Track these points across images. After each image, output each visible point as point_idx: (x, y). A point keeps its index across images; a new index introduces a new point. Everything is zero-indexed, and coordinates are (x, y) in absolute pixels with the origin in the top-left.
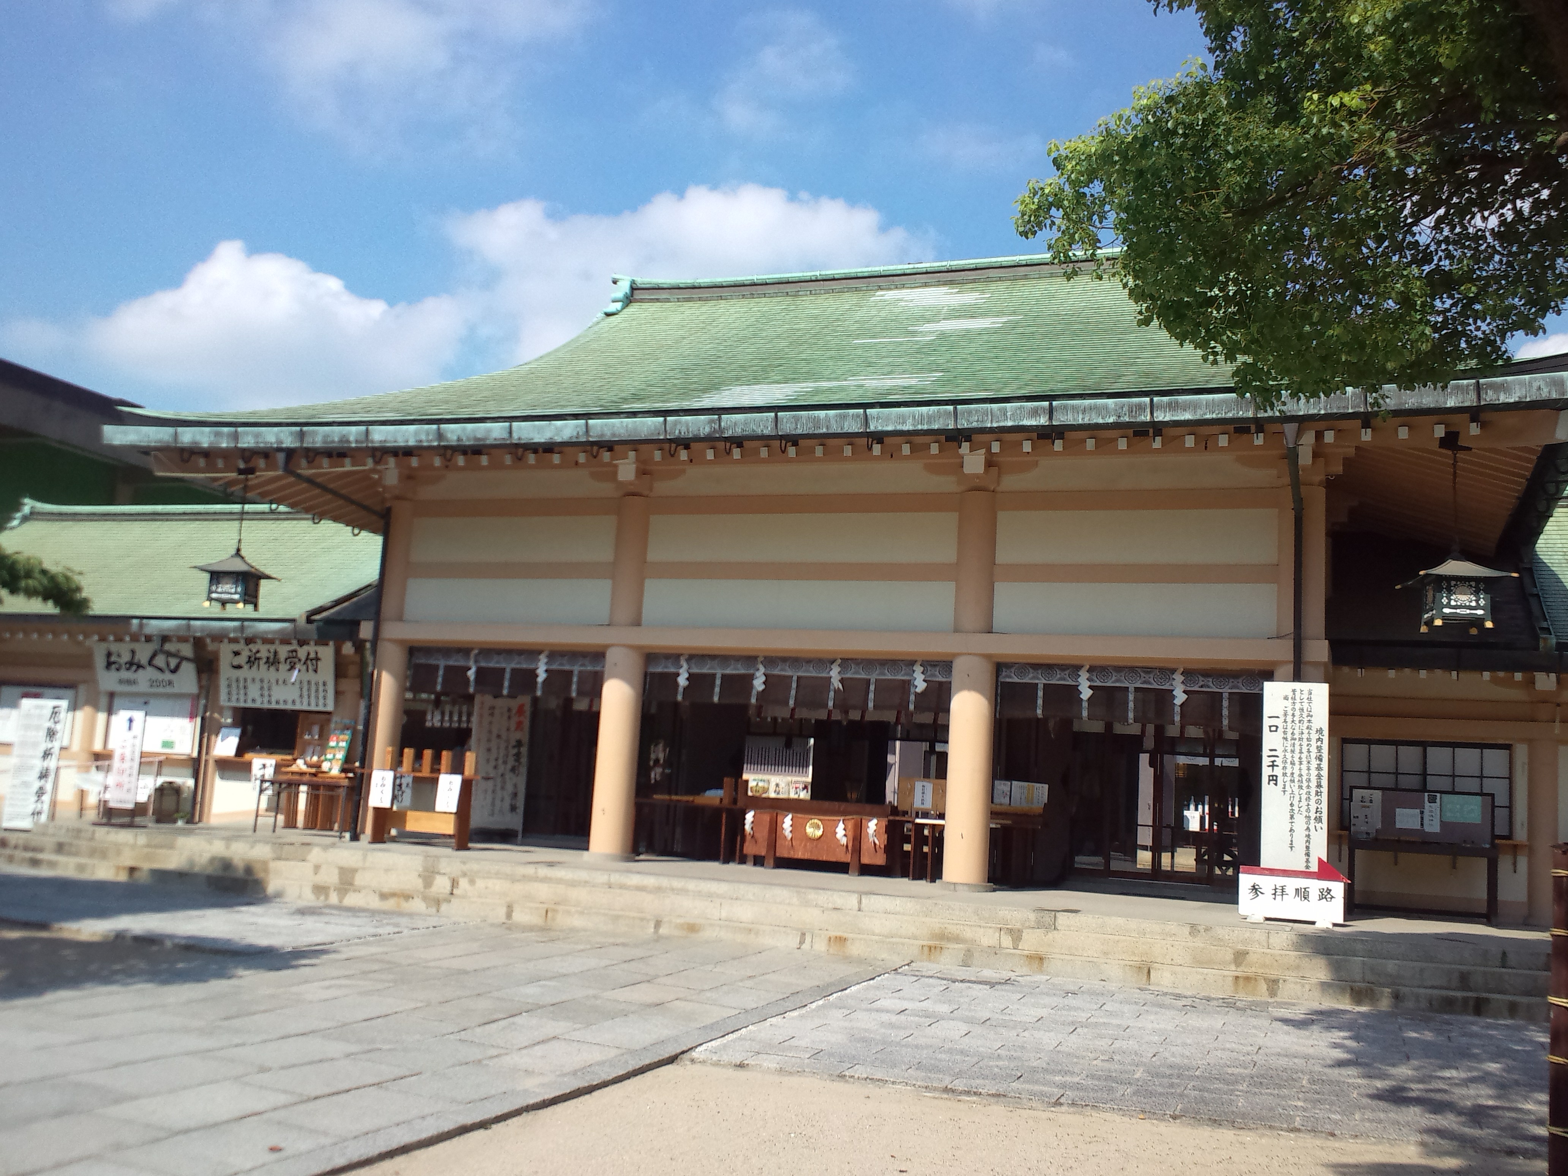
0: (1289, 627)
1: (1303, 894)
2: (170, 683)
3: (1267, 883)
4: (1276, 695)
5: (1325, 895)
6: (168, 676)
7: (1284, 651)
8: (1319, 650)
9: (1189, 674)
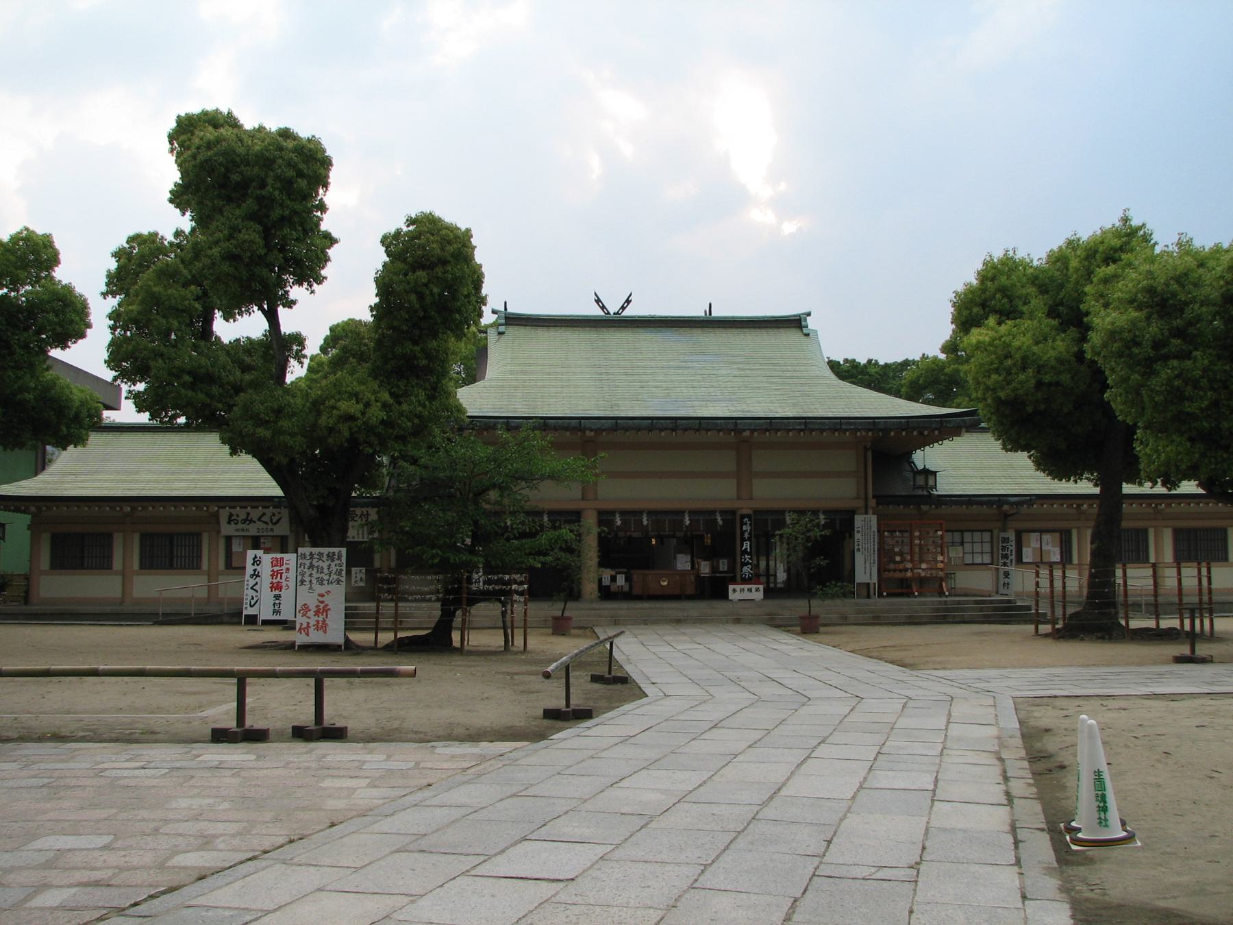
0: (863, 496)
1: (750, 590)
2: (272, 530)
3: (738, 587)
4: (859, 520)
5: (757, 590)
6: (270, 526)
7: (860, 503)
8: (872, 502)
9: (825, 512)
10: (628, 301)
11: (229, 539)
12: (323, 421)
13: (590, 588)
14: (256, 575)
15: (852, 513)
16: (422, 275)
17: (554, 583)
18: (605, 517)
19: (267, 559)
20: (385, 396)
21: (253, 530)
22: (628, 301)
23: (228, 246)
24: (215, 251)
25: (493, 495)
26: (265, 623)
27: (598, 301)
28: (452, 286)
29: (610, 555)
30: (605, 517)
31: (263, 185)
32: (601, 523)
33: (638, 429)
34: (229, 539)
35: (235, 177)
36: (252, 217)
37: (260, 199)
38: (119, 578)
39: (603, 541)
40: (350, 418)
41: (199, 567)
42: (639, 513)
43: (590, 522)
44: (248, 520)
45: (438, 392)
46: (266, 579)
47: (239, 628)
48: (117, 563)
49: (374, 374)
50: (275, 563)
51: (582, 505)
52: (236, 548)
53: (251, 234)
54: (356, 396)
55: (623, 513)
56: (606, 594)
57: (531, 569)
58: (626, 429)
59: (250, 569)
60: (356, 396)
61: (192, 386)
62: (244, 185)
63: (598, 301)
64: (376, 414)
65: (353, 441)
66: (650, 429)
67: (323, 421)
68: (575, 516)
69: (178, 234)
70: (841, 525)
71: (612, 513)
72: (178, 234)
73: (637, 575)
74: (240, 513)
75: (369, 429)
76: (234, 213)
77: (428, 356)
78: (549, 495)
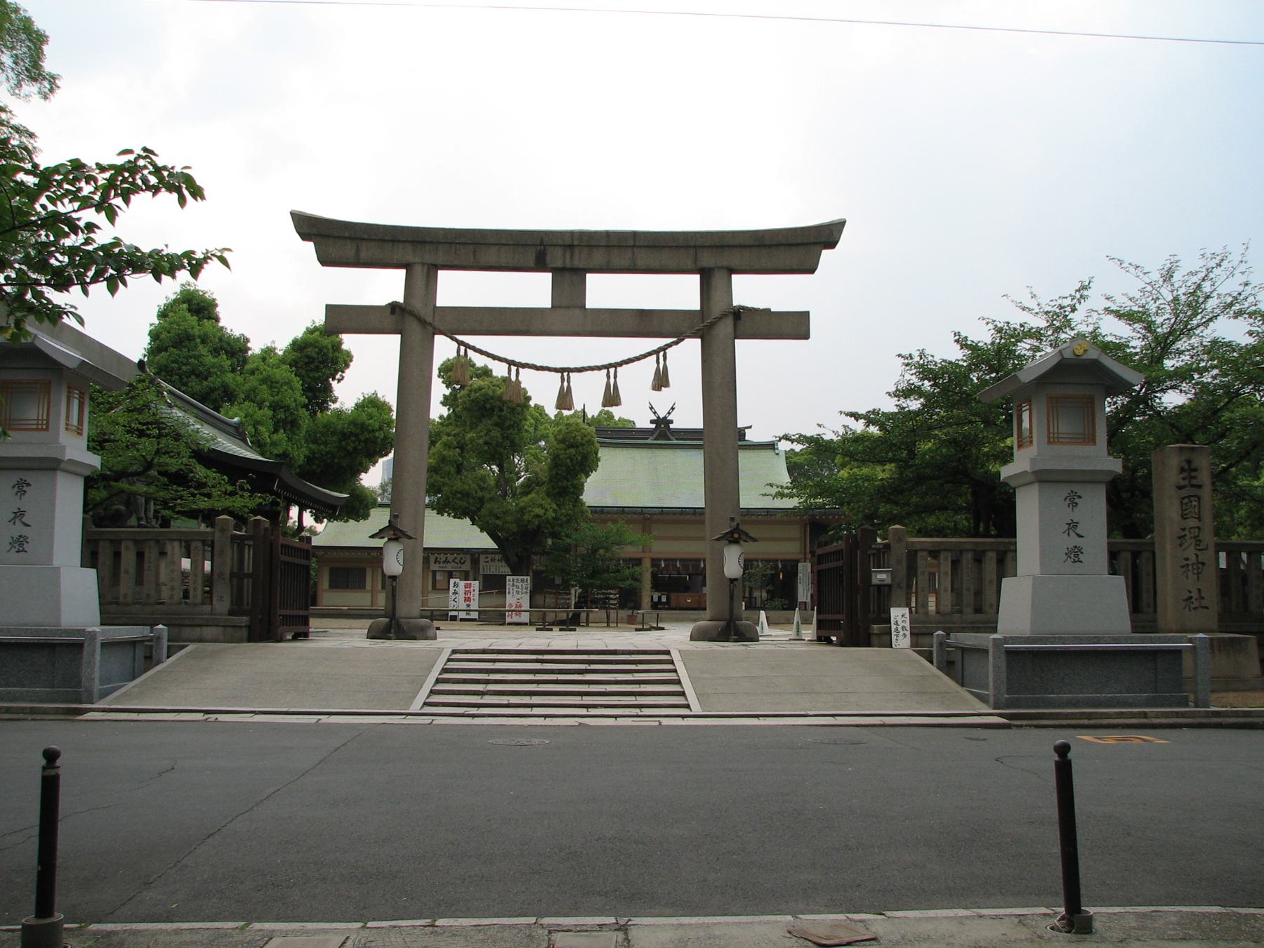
8: (809, 556)
10: (673, 409)
11: (434, 573)
12: (526, 517)
13: (646, 601)
14: (455, 593)
15: (797, 561)
16: (572, 451)
17: (629, 600)
18: (655, 562)
19: (462, 583)
20: (554, 506)
21: (449, 567)
22: (673, 409)
23: (486, 438)
24: (481, 441)
25: (601, 551)
26: (462, 620)
27: (651, 408)
28: (585, 457)
29: (657, 584)
30: (655, 562)
31: (502, 410)
32: (653, 566)
33: (674, 514)
34: (434, 573)
35: (488, 406)
36: (496, 424)
37: (499, 417)
38: (369, 595)
39: (654, 575)
40: (538, 516)
41: (364, 587)
42: (675, 560)
43: (647, 564)
44: (446, 561)
45: (577, 502)
46: (462, 596)
47: (783, 557)
48: (368, 586)
49: (548, 494)
50: (467, 586)
51: (642, 555)
52: (439, 577)
53: (496, 433)
54: (541, 506)
55: (665, 560)
56: (655, 606)
57: (620, 588)
58: (668, 514)
59: (452, 589)
60: (541, 506)
61: (460, 499)
62: (492, 409)
63: (651, 408)
64: (551, 514)
65: (539, 527)
66: (681, 513)
67: (526, 517)
68: (638, 562)
69: (441, 417)
70: (791, 569)
71: (660, 560)
72: (441, 417)
73: (673, 596)
74: (450, 557)
75: (547, 521)
76: (488, 422)
77: (574, 487)
78: (629, 551)
